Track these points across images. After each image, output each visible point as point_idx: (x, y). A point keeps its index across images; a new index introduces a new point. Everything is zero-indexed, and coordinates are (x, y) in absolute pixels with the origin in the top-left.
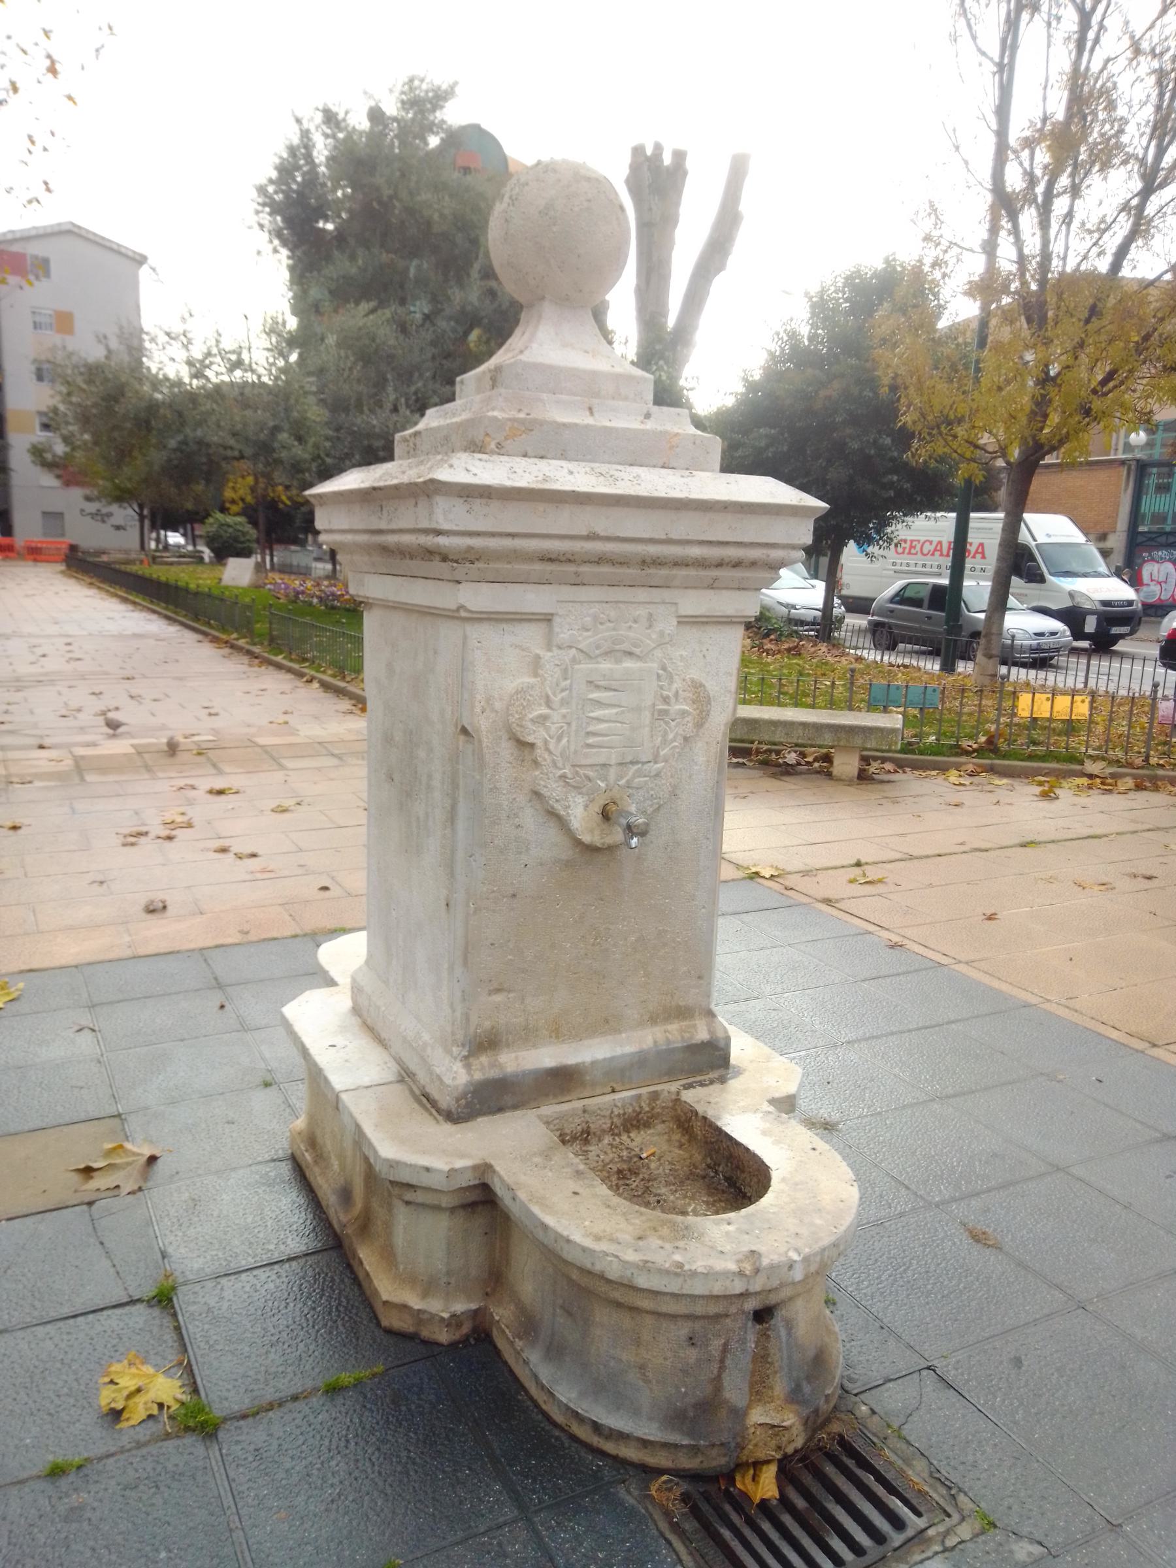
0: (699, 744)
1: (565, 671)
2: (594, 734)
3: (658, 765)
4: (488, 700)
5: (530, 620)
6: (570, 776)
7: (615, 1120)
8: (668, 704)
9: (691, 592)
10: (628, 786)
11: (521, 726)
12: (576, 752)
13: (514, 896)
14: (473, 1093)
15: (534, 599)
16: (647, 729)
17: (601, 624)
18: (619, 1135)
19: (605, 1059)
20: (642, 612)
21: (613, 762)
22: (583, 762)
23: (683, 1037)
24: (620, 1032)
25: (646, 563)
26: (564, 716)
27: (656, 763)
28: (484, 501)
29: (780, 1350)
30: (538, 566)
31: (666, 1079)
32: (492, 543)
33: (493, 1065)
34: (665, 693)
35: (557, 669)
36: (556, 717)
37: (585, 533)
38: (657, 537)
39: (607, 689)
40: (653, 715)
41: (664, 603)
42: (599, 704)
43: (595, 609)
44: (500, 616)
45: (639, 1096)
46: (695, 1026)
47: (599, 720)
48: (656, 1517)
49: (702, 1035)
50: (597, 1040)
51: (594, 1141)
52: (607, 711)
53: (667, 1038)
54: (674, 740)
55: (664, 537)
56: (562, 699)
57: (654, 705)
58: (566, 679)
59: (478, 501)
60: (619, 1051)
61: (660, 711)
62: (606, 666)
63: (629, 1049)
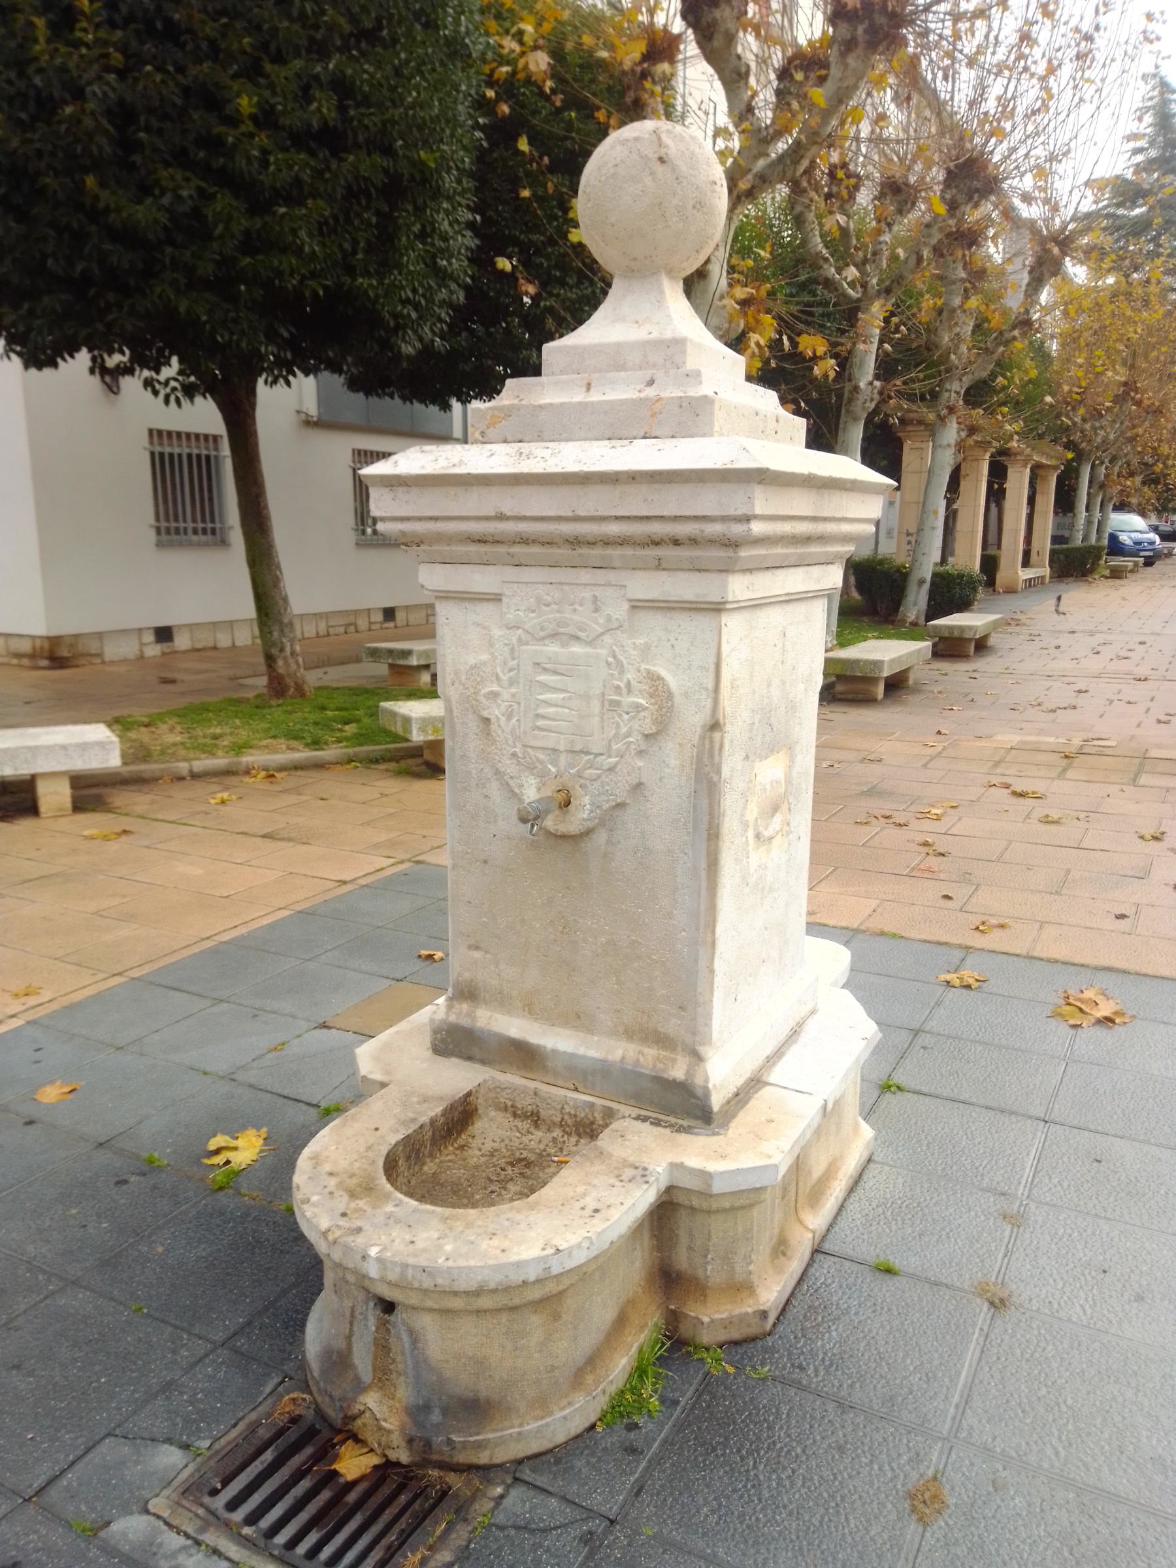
0: (670, 745)
1: (512, 651)
2: (544, 717)
3: (610, 760)
4: (456, 673)
5: (488, 600)
6: (520, 755)
7: (566, 1117)
8: (620, 694)
9: (640, 574)
10: (579, 775)
11: (476, 700)
12: (525, 732)
13: (485, 862)
14: (448, 1032)
15: (481, 579)
16: (597, 719)
17: (547, 605)
18: (569, 1134)
19: (565, 1053)
20: (587, 594)
21: (562, 748)
22: (532, 744)
23: (655, 1066)
24: (593, 1034)
25: (575, 542)
26: (513, 696)
27: (610, 756)
28: (405, 489)
29: (403, 1353)
30: (473, 548)
31: (632, 1102)
32: (419, 527)
33: (469, 1015)
34: (616, 682)
35: (506, 649)
36: (506, 695)
37: (493, 514)
38: (563, 514)
39: (555, 672)
40: (603, 705)
41: (610, 585)
42: (546, 687)
43: (540, 590)
44: (465, 596)
45: (592, 1105)
46: (674, 1061)
47: (548, 703)
48: (259, 1409)
49: (678, 1072)
50: (567, 1032)
51: (544, 1127)
52: (554, 696)
53: (638, 1060)
54: (628, 735)
55: (570, 514)
56: (510, 678)
57: (603, 695)
58: (513, 659)
59: (401, 489)
60: (582, 1051)
61: (611, 702)
62: (552, 648)
63: (593, 1053)
